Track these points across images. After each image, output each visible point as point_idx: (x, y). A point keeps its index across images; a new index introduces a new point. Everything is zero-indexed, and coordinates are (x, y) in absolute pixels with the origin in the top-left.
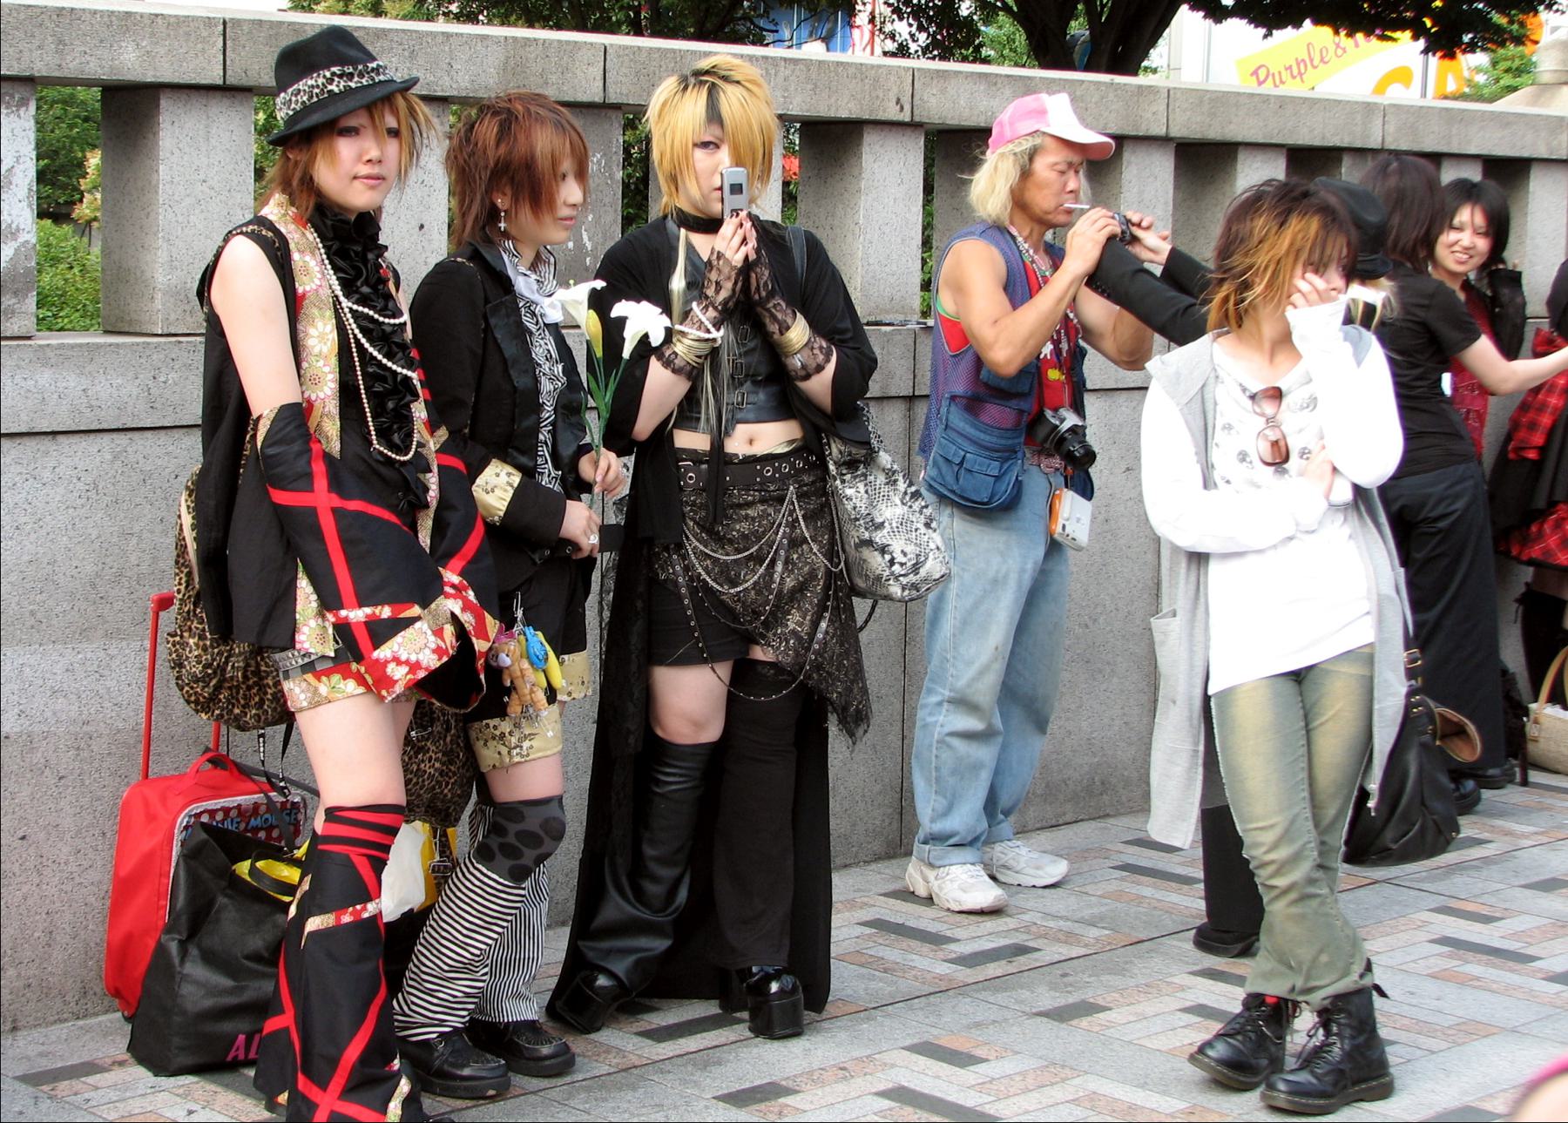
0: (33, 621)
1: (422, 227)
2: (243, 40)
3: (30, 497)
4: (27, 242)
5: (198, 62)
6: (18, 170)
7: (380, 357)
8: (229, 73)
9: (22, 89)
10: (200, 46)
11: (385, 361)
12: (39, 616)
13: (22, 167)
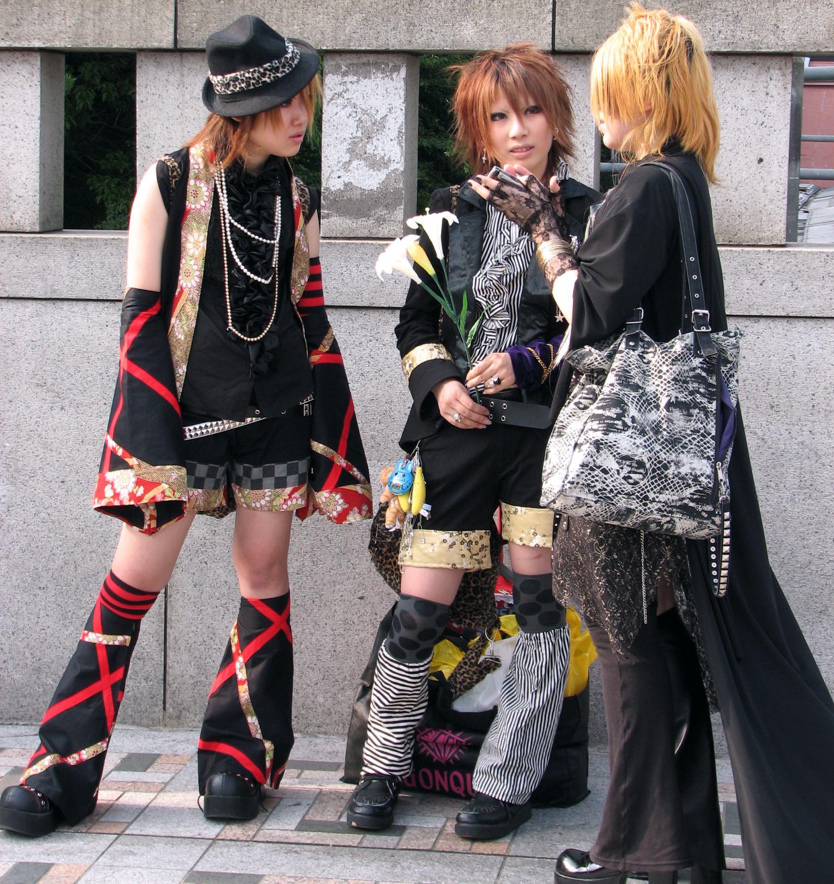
0: (373, 443)
1: (761, 160)
2: (570, 15)
3: (373, 353)
4: (397, 169)
5: (529, 34)
6: (390, 118)
7: (240, 264)
8: (557, 41)
9: (395, 59)
10: (531, 22)
11: (242, 267)
12: (378, 439)
13: (394, 115)
